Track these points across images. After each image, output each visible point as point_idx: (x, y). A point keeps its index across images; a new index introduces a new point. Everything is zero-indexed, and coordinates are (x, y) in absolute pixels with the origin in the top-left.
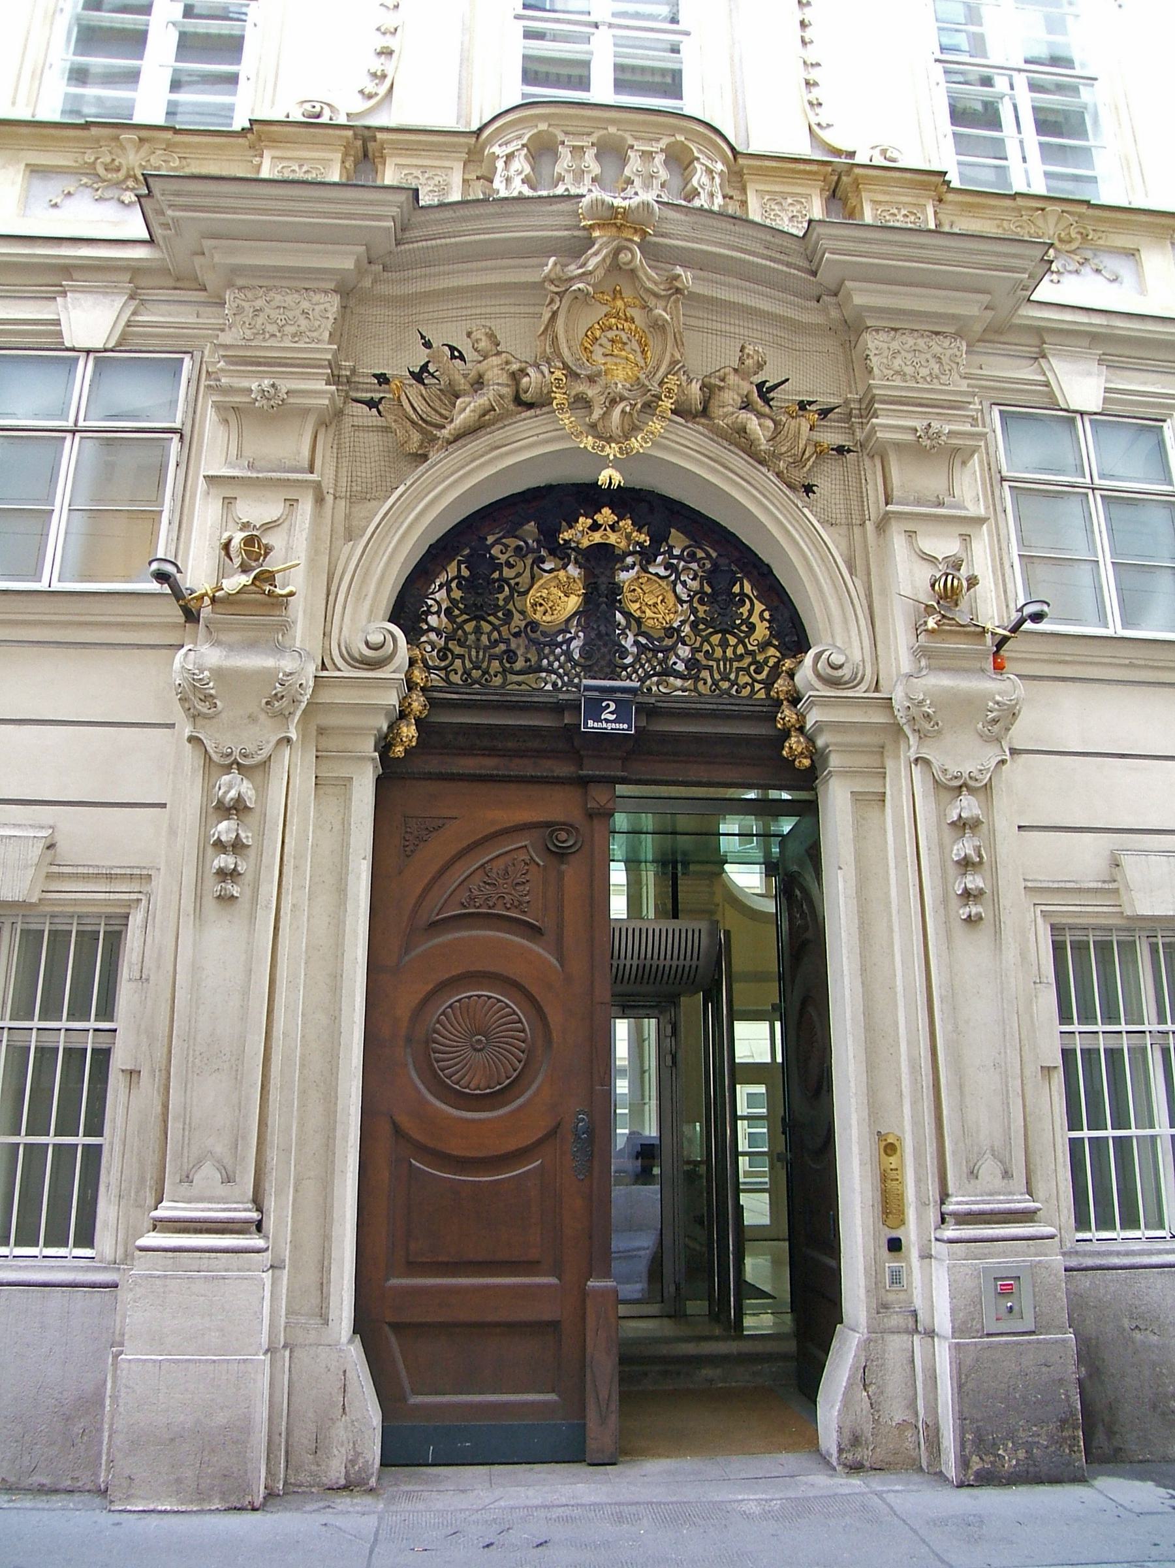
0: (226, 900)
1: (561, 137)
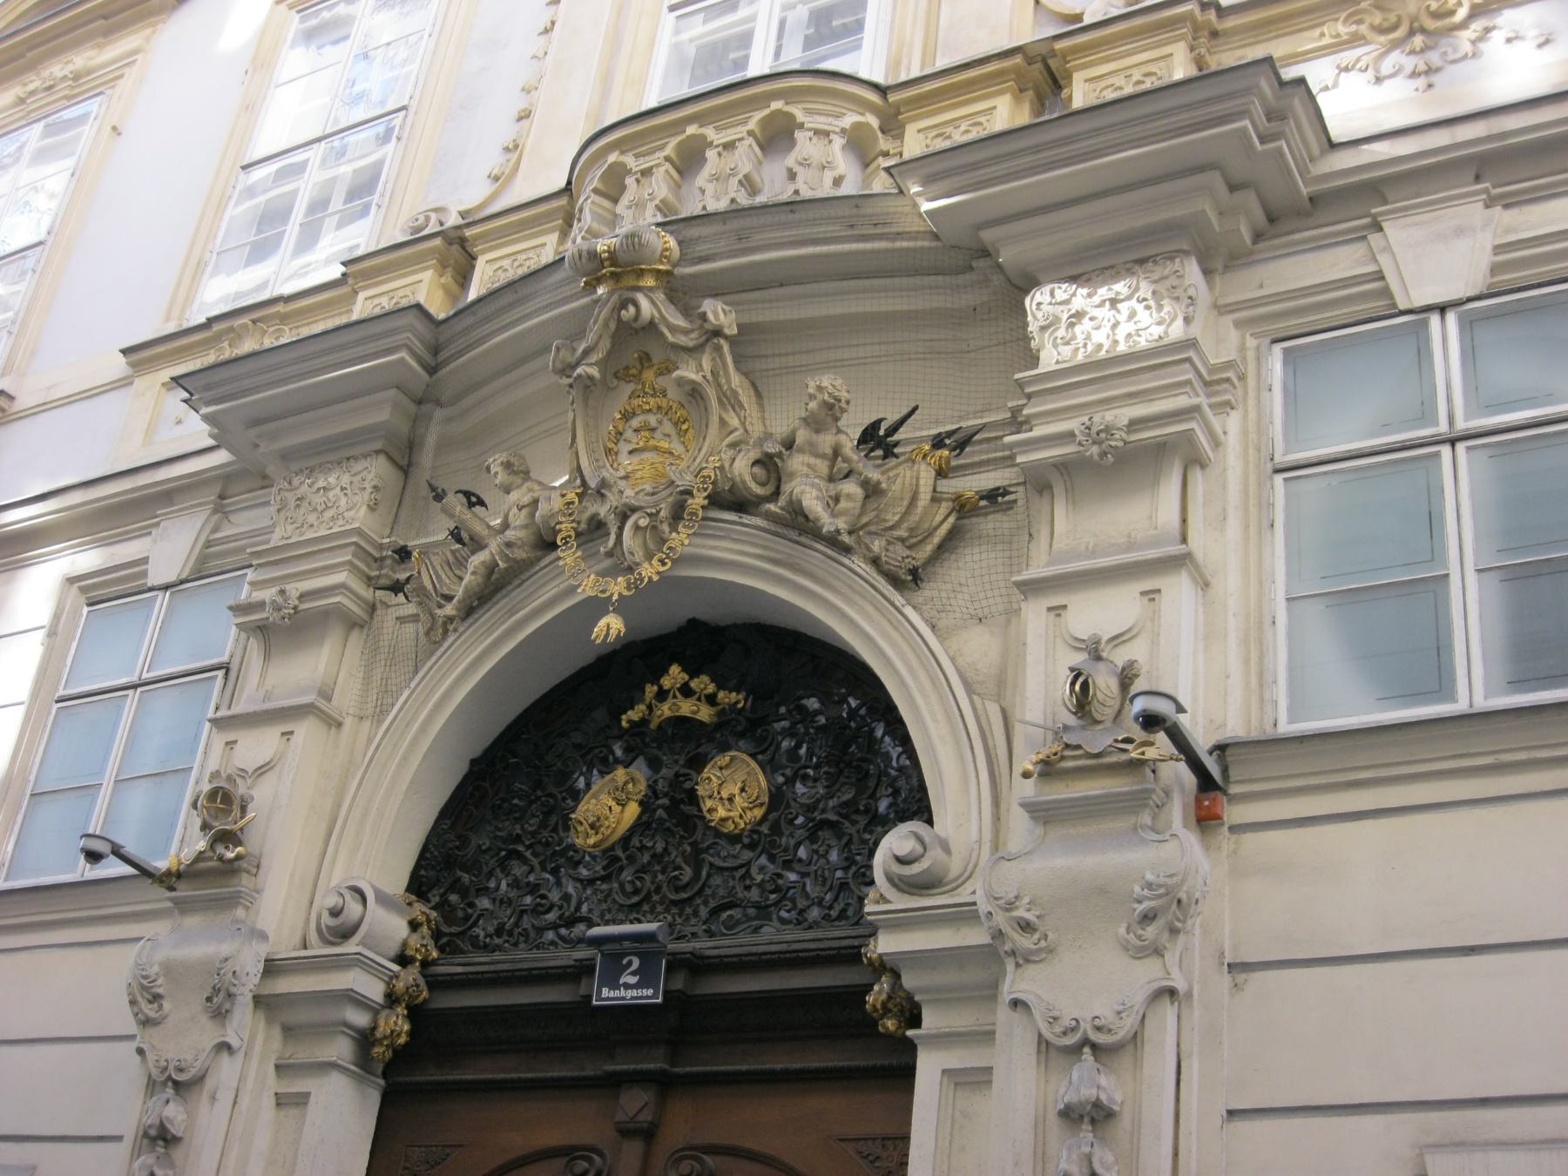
1: (800, 116)
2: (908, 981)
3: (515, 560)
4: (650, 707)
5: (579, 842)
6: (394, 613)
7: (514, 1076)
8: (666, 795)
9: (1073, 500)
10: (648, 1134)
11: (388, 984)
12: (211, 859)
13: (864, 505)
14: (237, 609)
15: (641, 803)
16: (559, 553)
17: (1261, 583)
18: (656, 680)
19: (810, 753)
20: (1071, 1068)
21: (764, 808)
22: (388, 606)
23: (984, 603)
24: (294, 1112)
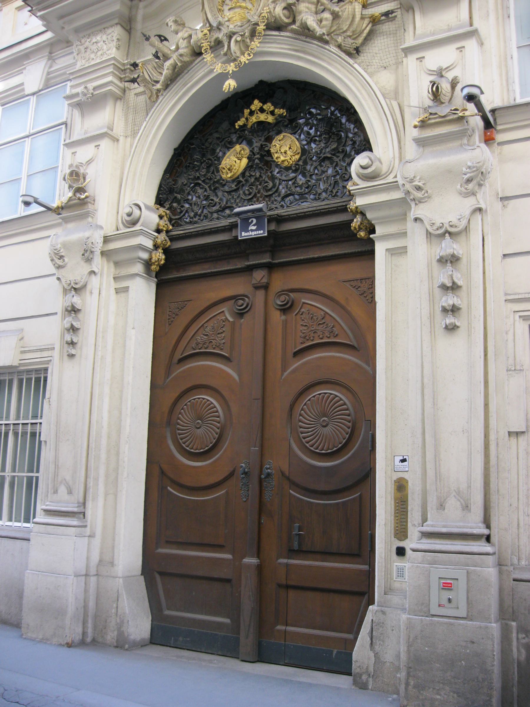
0: (451, 329)
2: (369, 216)
3: (184, 62)
4: (247, 119)
5: (224, 176)
6: (133, 92)
7: (209, 271)
8: (258, 153)
9: (423, 12)
10: (266, 287)
11: (154, 241)
12: (75, 199)
13: (332, 23)
14: (68, 98)
15: (248, 158)
16: (204, 56)
17: (505, 42)
18: (248, 107)
19: (316, 131)
20: (441, 243)
21: (300, 155)
22: (130, 90)
23: (387, 60)
24: (123, 295)
